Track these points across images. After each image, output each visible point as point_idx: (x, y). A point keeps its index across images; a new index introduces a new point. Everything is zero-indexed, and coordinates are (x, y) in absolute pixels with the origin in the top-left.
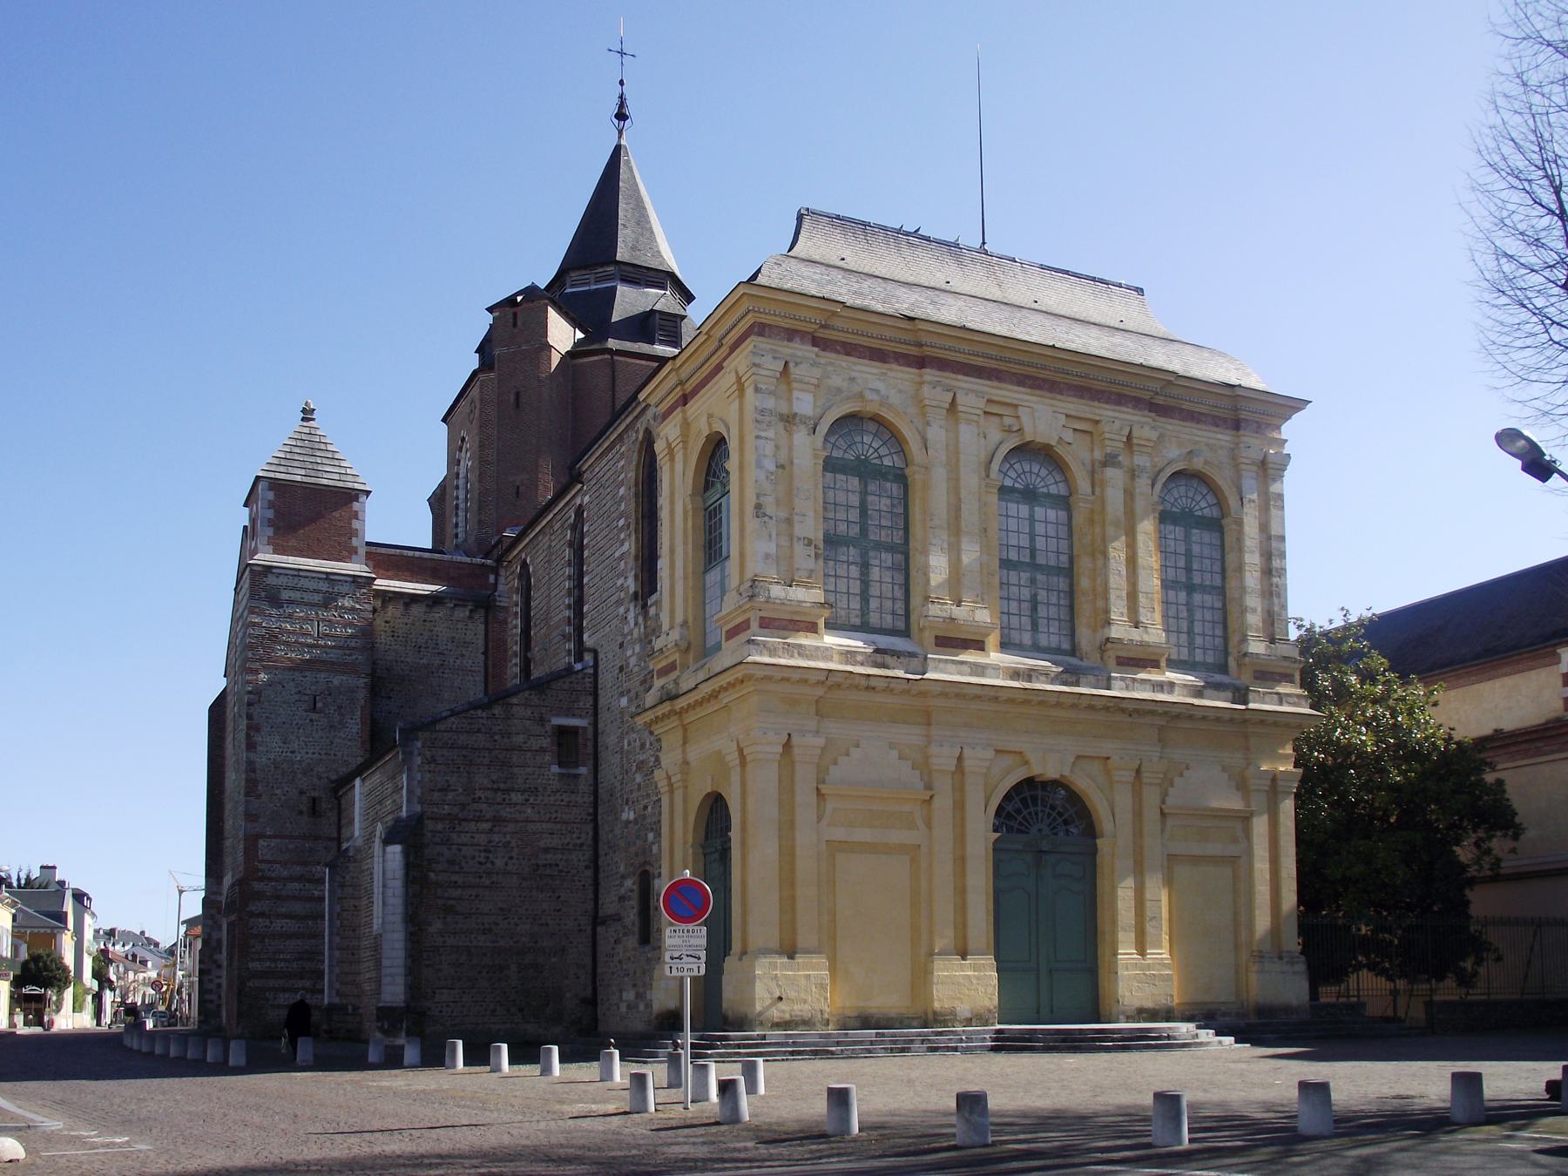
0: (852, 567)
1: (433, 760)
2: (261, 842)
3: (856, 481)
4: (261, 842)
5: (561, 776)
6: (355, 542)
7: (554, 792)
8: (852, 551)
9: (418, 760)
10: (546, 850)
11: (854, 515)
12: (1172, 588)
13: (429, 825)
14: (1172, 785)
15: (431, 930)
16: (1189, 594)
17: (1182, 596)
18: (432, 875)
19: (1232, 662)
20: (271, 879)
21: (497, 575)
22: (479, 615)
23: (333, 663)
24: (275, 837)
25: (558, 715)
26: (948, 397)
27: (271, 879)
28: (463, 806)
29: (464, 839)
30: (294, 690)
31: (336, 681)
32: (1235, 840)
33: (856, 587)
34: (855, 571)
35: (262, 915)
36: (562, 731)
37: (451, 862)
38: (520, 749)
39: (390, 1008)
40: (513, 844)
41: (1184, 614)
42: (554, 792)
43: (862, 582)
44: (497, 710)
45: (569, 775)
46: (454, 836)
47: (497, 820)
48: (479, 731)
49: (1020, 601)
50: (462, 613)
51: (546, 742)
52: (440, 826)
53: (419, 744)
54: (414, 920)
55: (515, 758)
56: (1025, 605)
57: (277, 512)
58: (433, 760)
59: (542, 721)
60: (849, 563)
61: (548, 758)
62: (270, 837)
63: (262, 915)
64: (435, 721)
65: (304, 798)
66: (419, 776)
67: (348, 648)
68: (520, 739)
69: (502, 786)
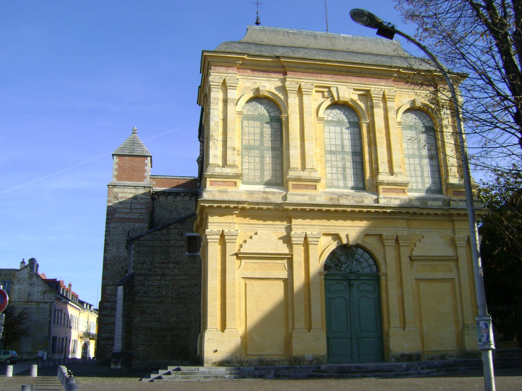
0: (257, 158)
1: (139, 252)
2: (107, 287)
3: (258, 123)
4: (107, 287)
5: (190, 256)
6: (146, 174)
7: (186, 263)
8: (256, 151)
9: (133, 252)
10: (183, 287)
11: (257, 137)
12: (412, 158)
13: (137, 278)
14: (415, 246)
15: (136, 320)
16: (420, 160)
17: (417, 161)
18: (137, 298)
19: (444, 188)
20: (110, 302)
21: (200, 183)
22: (193, 198)
23: (135, 219)
24: (112, 285)
25: (188, 232)
26: (298, 86)
27: (110, 302)
28: (150, 270)
29: (150, 283)
30: (121, 230)
31: (137, 226)
32: (451, 270)
33: (258, 166)
34: (258, 160)
35: (107, 315)
36: (190, 238)
37: (145, 293)
38: (173, 246)
39: (117, 353)
40: (170, 284)
41: (419, 168)
42: (186, 263)
43: (261, 164)
44: (164, 231)
45: (192, 256)
46: (146, 282)
47: (163, 275)
48: (157, 239)
49: (337, 167)
50: (187, 198)
51: (183, 243)
52: (140, 278)
53: (134, 246)
54: (127, 316)
55: (171, 250)
56: (339, 169)
57: (119, 166)
58: (139, 252)
59: (182, 234)
60: (255, 157)
61: (184, 249)
62: (111, 285)
63: (107, 315)
64: (140, 236)
65: (123, 270)
66: (133, 258)
67: (141, 213)
68: (173, 242)
69: (165, 261)
